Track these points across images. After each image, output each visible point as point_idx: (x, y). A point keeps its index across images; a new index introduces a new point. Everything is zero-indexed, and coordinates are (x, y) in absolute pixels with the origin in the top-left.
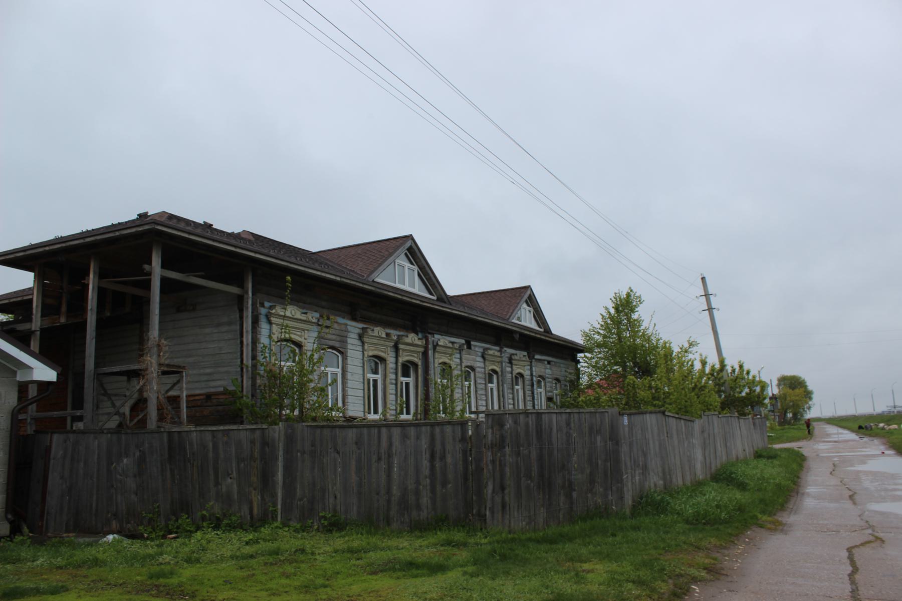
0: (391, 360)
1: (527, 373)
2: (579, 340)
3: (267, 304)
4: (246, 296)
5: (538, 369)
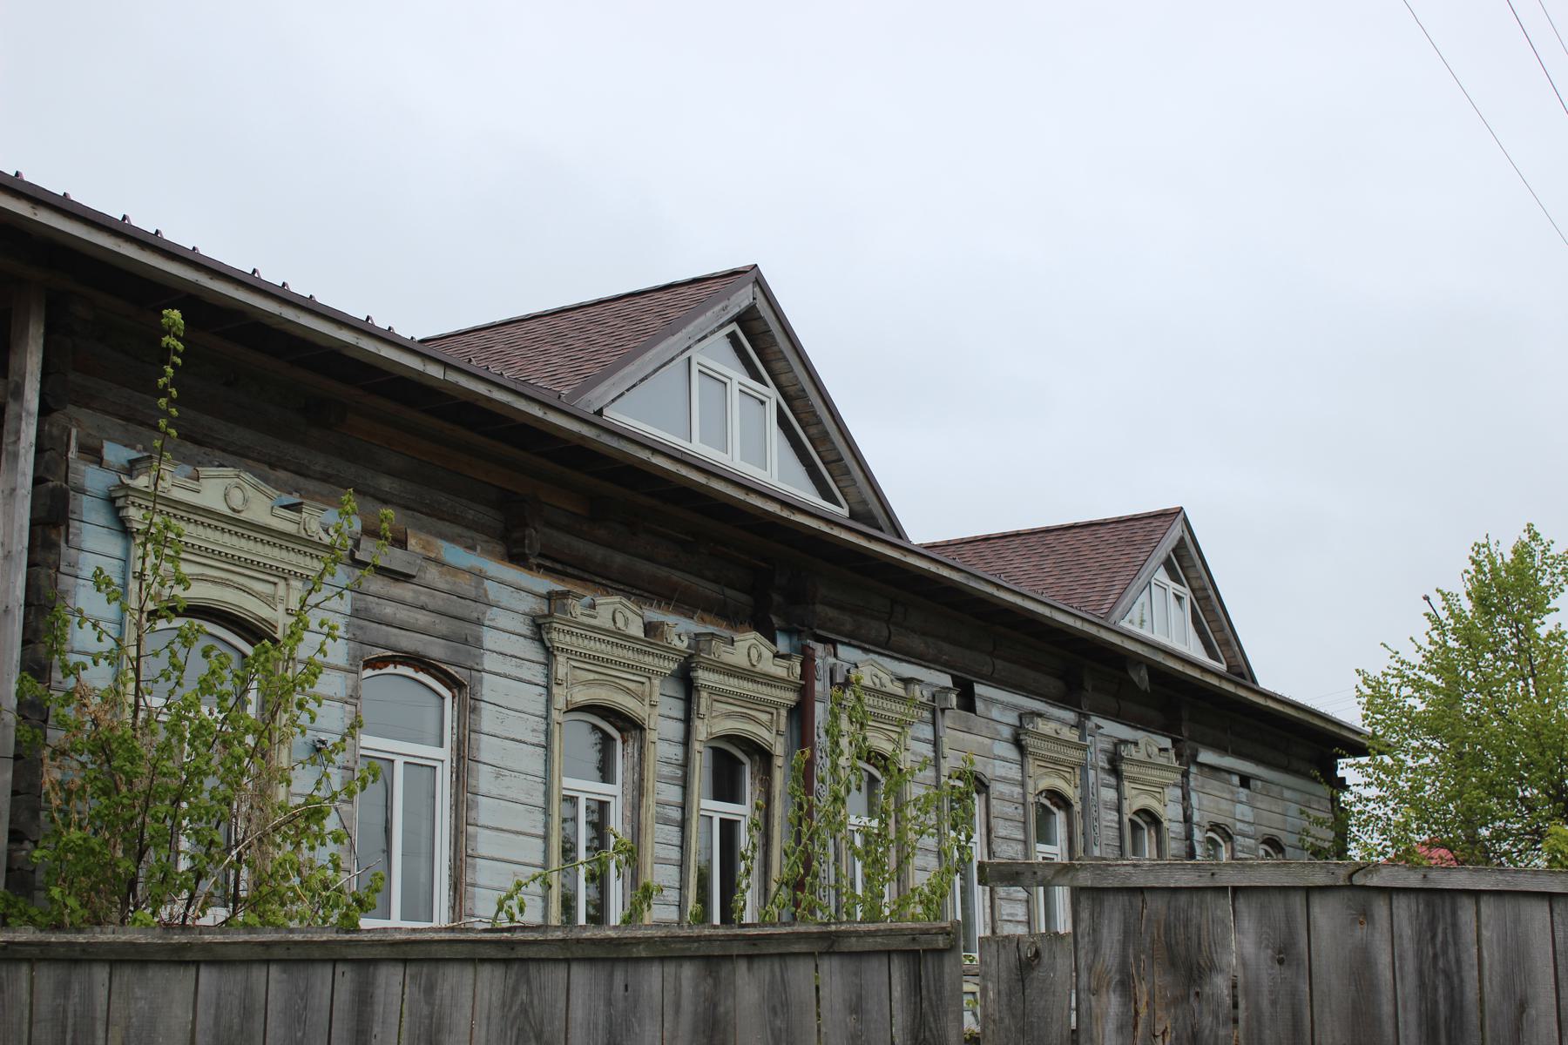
0: (663, 725)
1: (1170, 813)
2: (1348, 711)
3: (116, 453)
4: (12, 408)
5: (1212, 802)
